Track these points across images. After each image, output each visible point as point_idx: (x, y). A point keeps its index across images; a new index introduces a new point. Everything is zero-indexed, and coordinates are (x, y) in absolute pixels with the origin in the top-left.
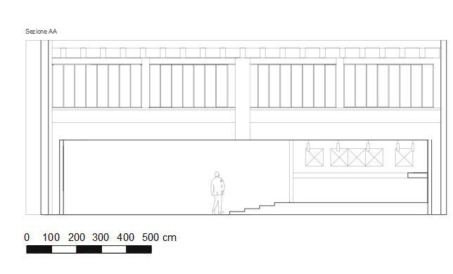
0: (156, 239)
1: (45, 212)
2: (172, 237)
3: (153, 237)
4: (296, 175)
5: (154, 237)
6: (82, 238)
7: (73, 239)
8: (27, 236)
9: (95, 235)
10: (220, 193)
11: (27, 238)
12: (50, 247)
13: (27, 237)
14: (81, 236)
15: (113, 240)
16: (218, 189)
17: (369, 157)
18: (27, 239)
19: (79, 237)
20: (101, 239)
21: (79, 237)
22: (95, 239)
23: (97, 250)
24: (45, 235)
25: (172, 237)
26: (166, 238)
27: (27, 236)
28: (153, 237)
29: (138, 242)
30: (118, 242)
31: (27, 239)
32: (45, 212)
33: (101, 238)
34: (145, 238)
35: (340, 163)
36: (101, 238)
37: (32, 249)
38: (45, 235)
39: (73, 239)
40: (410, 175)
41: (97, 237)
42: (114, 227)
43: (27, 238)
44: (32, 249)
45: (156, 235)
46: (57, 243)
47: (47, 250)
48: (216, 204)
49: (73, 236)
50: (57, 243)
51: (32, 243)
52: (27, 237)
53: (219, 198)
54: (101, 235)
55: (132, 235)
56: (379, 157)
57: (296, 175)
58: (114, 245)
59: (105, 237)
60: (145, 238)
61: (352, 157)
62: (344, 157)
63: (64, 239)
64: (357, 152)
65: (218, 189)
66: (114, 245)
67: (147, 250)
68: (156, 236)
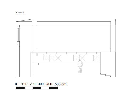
0: (26, 84)
1: (18, 75)
2: (65, 84)
3: (59, 84)
4: (33, 64)
5: (59, 84)
6: (34, 84)
7: (31, 84)
8: (16, 84)
9: (39, 83)
10: (81, 66)
11: (16, 84)
12: (24, 87)
13: (16, 84)
14: (34, 84)
15: (45, 85)
16: (81, 65)
17: (56, 58)
18: (16, 84)
19: (34, 84)
20: (58, 85)
21: (34, 84)
22: (39, 84)
23: (39, 88)
24: (22, 83)
25: (65, 84)
26: (62, 85)
27: (16, 84)
28: (59, 84)
29: (53, 85)
30: (47, 86)
31: (16, 84)
32: (18, 75)
33: (41, 84)
34: (56, 85)
35: (47, 60)
36: (41, 84)
37: (18, 88)
38: (22, 83)
39: (31, 84)
40: (38, 64)
41: (40, 84)
42: (45, 81)
43: (16, 84)
44: (18, 88)
45: (26, 83)
46: (26, 86)
47: (23, 88)
48: (80, 69)
49: (31, 84)
50: (26, 86)
51: (18, 86)
52: (16, 84)
53: (81, 68)
54: (49, 83)
55: (43, 83)
56: (60, 58)
57: (33, 64)
58: (45, 87)
59: (42, 84)
60: (56, 85)
61: (51, 58)
62: (48, 58)
63: (29, 85)
64: (52, 56)
65: (81, 65)
66: (45, 87)
67: (56, 88)
68: (43, 84)
